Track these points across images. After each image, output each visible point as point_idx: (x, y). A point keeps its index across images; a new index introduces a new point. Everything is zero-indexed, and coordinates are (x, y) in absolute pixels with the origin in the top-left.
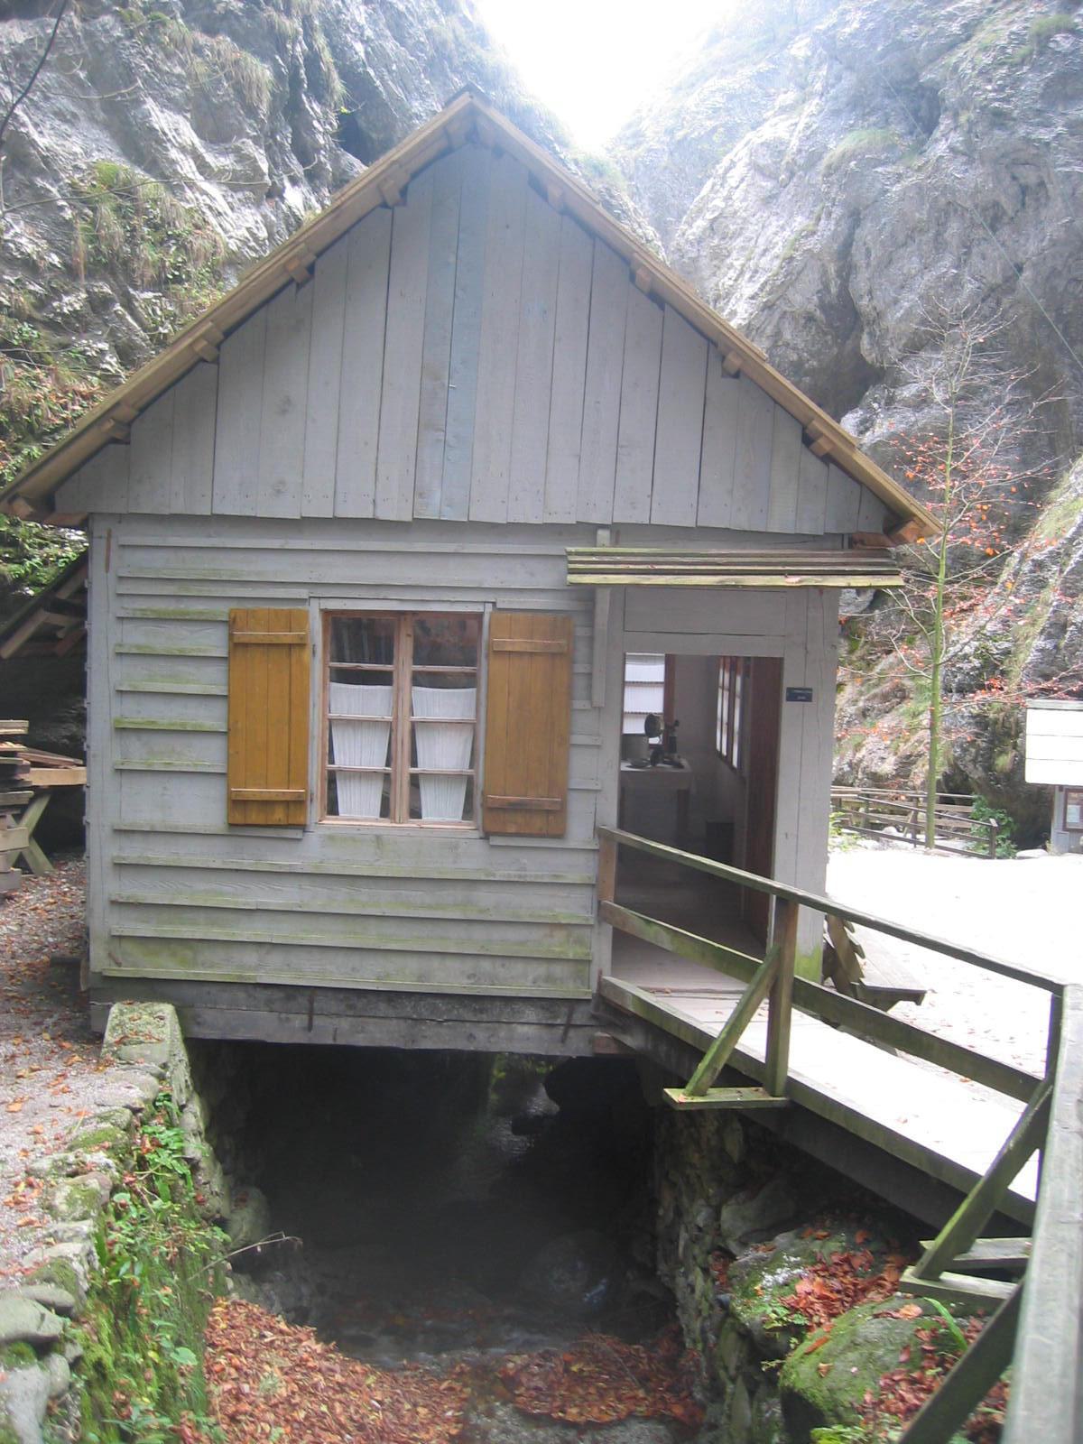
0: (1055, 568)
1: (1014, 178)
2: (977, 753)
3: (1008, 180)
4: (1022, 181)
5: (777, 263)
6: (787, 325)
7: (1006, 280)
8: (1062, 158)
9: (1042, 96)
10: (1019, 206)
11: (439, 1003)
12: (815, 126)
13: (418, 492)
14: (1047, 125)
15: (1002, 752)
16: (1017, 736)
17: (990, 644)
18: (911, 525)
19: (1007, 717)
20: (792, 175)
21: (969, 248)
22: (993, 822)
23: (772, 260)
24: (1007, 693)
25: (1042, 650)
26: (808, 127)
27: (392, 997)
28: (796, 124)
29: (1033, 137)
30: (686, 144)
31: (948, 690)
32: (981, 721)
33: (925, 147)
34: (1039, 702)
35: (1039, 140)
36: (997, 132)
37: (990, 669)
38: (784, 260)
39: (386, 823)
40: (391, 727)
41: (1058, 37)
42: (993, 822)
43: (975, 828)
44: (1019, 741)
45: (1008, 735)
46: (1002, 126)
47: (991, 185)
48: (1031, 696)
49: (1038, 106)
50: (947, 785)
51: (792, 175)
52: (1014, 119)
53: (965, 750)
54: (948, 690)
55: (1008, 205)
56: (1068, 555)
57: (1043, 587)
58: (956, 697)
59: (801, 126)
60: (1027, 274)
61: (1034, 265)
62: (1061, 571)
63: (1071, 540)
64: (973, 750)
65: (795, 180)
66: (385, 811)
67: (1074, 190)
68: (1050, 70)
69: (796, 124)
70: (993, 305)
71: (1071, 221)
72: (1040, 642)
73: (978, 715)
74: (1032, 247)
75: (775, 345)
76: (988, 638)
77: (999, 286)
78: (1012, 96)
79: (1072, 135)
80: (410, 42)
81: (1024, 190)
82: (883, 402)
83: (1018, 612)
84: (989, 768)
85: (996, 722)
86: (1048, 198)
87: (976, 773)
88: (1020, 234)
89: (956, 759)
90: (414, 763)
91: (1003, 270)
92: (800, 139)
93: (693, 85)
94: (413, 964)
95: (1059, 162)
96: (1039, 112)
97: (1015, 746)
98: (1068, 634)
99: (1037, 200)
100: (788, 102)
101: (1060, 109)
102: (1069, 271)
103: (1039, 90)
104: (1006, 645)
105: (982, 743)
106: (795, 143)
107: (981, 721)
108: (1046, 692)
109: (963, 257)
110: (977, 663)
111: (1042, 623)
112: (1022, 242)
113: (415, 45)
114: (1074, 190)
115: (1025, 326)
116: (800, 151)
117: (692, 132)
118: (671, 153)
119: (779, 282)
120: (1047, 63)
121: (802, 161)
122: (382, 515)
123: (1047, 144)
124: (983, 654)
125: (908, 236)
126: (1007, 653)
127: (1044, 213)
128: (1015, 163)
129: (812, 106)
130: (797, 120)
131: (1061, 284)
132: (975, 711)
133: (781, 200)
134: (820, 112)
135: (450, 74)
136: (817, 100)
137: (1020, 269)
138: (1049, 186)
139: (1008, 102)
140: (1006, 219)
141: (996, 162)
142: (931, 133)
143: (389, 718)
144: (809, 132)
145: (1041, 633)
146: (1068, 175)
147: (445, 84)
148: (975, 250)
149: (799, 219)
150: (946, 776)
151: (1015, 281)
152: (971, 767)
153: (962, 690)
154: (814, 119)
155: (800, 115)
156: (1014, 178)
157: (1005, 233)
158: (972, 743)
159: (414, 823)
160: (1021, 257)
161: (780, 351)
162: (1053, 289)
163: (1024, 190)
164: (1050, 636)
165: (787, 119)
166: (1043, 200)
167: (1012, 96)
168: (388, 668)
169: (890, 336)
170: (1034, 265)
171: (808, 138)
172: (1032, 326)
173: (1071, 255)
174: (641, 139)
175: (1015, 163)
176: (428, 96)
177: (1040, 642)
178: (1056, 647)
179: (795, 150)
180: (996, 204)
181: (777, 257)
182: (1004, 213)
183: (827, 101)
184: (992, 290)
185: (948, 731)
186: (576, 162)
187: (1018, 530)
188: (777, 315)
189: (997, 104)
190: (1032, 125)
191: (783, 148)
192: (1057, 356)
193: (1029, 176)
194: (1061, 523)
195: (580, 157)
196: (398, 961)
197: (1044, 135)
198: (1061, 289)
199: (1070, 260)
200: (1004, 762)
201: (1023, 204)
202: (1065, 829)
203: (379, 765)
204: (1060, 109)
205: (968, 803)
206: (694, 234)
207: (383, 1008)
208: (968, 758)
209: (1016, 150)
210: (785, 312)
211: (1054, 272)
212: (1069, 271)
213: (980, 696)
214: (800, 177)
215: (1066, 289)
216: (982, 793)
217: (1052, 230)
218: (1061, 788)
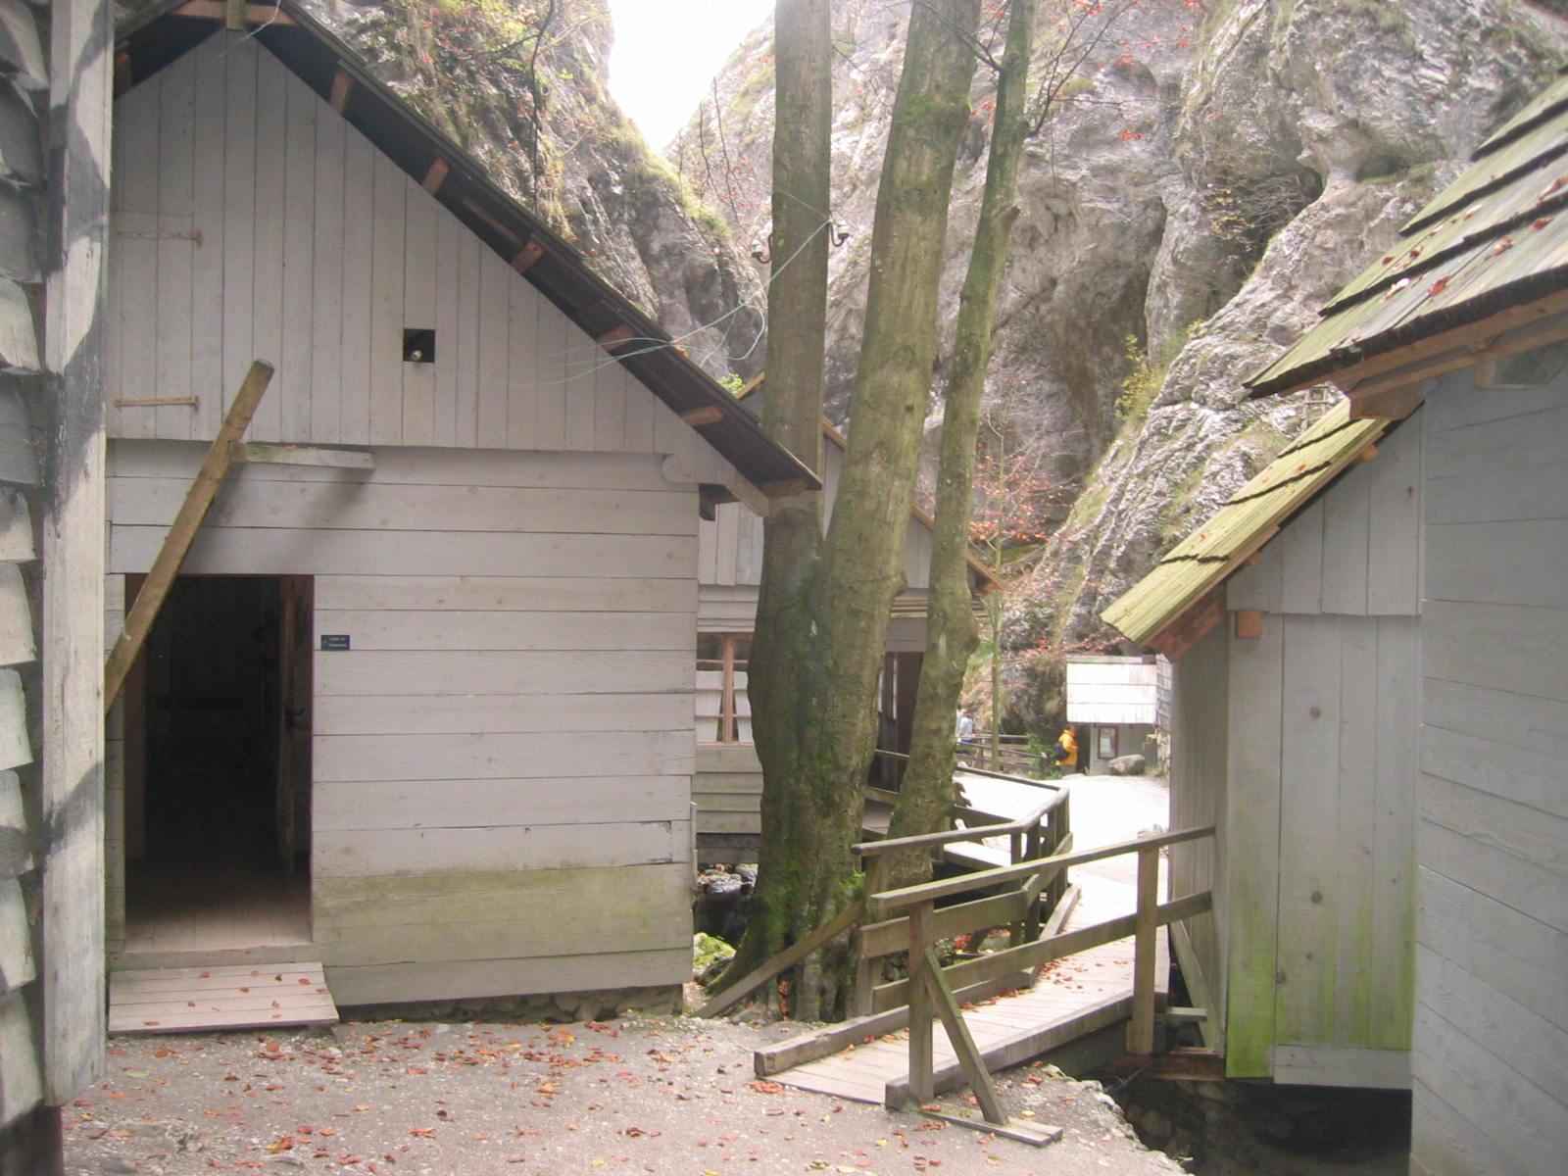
0: (1087, 548)
1: (1048, 208)
2: (1029, 699)
3: (1043, 208)
4: (1054, 211)
5: (843, 266)
6: (852, 321)
7: (1044, 290)
8: (1086, 195)
9: (1069, 144)
10: (1052, 231)
11: (752, 838)
12: (875, 148)
13: (739, 570)
14: (1074, 167)
15: (1050, 698)
16: (1061, 684)
17: (1037, 610)
18: (990, 585)
19: (1052, 670)
20: (855, 187)
21: (1011, 262)
22: (1044, 755)
23: (838, 263)
24: (1051, 651)
25: (1078, 615)
26: (869, 147)
27: (727, 836)
28: (857, 142)
29: (1063, 177)
30: (754, 147)
31: (1004, 648)
32: (1031, 673)
33: (972, 173)
34: (1076, 657)
35: (1068, 181)
36: (1032, 170)
37: (1038, 631)
38: (850, 264)
39: (720, 744)
40: (722, 693)
41: (1081, 97)
42: (1044, 755)
43: (1031, 762)
44: (1062, 689)
45: (1053, 684)
46: (1037, 166)
47: (1029, 213)
48: (1069, 652)
49: (1066, 152)
50: (1005, 729)
51: (855, 187)
52: (1047, 162)
53: (1019, 697)
54: (1004, 648)
55: (1043, 229)
56: (1096, 538)
57: (1077, 563)
58: (1010, 654)
59: (862, 145)
60: (1060, 288)
61: (1067, 281)
62: (1092, 552)
63: (1099, 527)
64: (1026, 698)
65: (858, 192)
66: (720, 738)
67: (1098, 222)
68: (1075, 123)
69: (857, 142)
70: (1033, 311)
71: (1096, 247)
72: (1076, 609)
73: (1029, 669)
74: (1064, 266)
75: (842, 338)
76: (1036, 605)
77: (1037, 295)
78: (1044, 142)
79: (1095, 176)
80: (565, 133)
81: (1056, 217)
82: (939, 392)
83: (1058, 586)
84: (1039, 711)
85: (1044, 673)
86: (1076, 225)
87: (1029, 717)
88: (1054, 254)
89: (1012, 705)
90: (734, 712)
91: (1041, 283)
92: (862, 159)
93: (759, 92)
94: (738, 818)
95: (1085, 199)
96: (1067, 157)
97: (1060, 693)
98: (1098, 603)
99: (1068, 227)
100: (849, 120)
101: (1084, 155)
102: (1096, 287)
103: (1067, 140)
104: (1050, 611)
105: (1033, 692)
106: (857, 159)
107: (1031, 673)
108: (1081, 650)
109: (1007, 270)
110: (1026, 626)
111: (1078, 592)
112: (1056, 260)
113: (569, 135)
114: (1098, 222)
115: (1061, 331)
116: (862, 168)
117: (760, 137)
118: (740, 155)
119: (845, 284)
120: (1071, 118)
121: (864, 178)
122: (719, 582)
123: (1074, 184)
124: (1034, 620)
125: (959, 249)
126: (1051, 617)
127: (1073, 239)
128: (1048, 195)
129: (871, 128)
130: (857, 138)
131: (1089, 297)
132: (1027, 665)
133: (846, 208)
134: (880, 134)
135: (594, 154)
136: (875, 124)
137: (1054, 283)
138: (1077, 217)
139: (1042, 147)
140: (1042, 241)
141: (1031, 194)
142: (976, 160)
143: (721, 688)
144: (869, 152)
145: (1077, 602)
146: (1093, 210)
147: (589, 161)
148: (1016, 265)
149: (862, 228)
150: (1004, 721)
151: (1051, 292)
152: (1024, 711)
153: (1016, 648)
154: (874, 140)
155: (861, 133)
156: (1048, 208)
157: (1041, 251)
158: (1024, 692)
159: (735, 744)
160: (1055, 273)
161: (847, 343)
162: (1083, 301)
163: (1056, 217)
164: (1083, 604)
165: (848, 136)
166: (1072, 228)
167: (1044, 142)
168: (721, 662)
169: (944, 333)
170: (1067, 281)
171: (869, 157)
172: (1066, 331)
173: (1096, 274)
174: (711, 138)
175: (1048, 195)
176: (578, 174)
177: (1076, 609)
178: (1089, 612)
179: (857, 167)
180: (1033, 228)
181: (843, 260)
182: (1040, 235)
183: (885, 126)
184: (1032, 298)
185: (1005, 682)
186: (693, 219)
187: (1053, 523)
188: (843, 312)
189: (1032, 148)
190: (1061, 167)
191: (846, 163)
192: (1088, 355)
193: (1061, 208)
194: (1091, 511)
195: (696, 215)
196: (729, 817)
197: (1071, 176)
198: (1089, 301)
199: (1096, 278)
200: (1051, 706)
201: (1056, 229)
202: (1099, 757)
203: (716, 712)
204: (1084, 155)
205: (1023, 742)
206: (765, 234)
207: (722, 843)
208: (1022, 704)
209: (1048, 186)
210: (851, 310)
211: (1083, 287)
212: (1096, 287)
213: (1029, 654)
214: (862, 191)
215: (1093, 302)
216: (1034, 732)
217: (1080, 253)
218: (1095, 725)
